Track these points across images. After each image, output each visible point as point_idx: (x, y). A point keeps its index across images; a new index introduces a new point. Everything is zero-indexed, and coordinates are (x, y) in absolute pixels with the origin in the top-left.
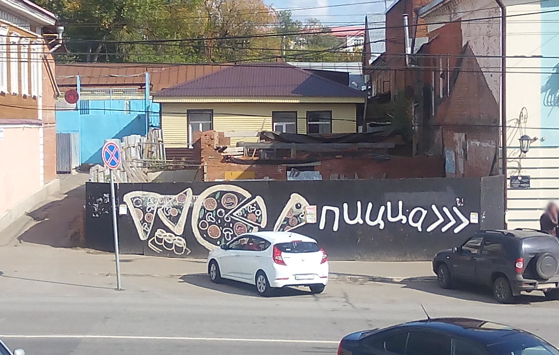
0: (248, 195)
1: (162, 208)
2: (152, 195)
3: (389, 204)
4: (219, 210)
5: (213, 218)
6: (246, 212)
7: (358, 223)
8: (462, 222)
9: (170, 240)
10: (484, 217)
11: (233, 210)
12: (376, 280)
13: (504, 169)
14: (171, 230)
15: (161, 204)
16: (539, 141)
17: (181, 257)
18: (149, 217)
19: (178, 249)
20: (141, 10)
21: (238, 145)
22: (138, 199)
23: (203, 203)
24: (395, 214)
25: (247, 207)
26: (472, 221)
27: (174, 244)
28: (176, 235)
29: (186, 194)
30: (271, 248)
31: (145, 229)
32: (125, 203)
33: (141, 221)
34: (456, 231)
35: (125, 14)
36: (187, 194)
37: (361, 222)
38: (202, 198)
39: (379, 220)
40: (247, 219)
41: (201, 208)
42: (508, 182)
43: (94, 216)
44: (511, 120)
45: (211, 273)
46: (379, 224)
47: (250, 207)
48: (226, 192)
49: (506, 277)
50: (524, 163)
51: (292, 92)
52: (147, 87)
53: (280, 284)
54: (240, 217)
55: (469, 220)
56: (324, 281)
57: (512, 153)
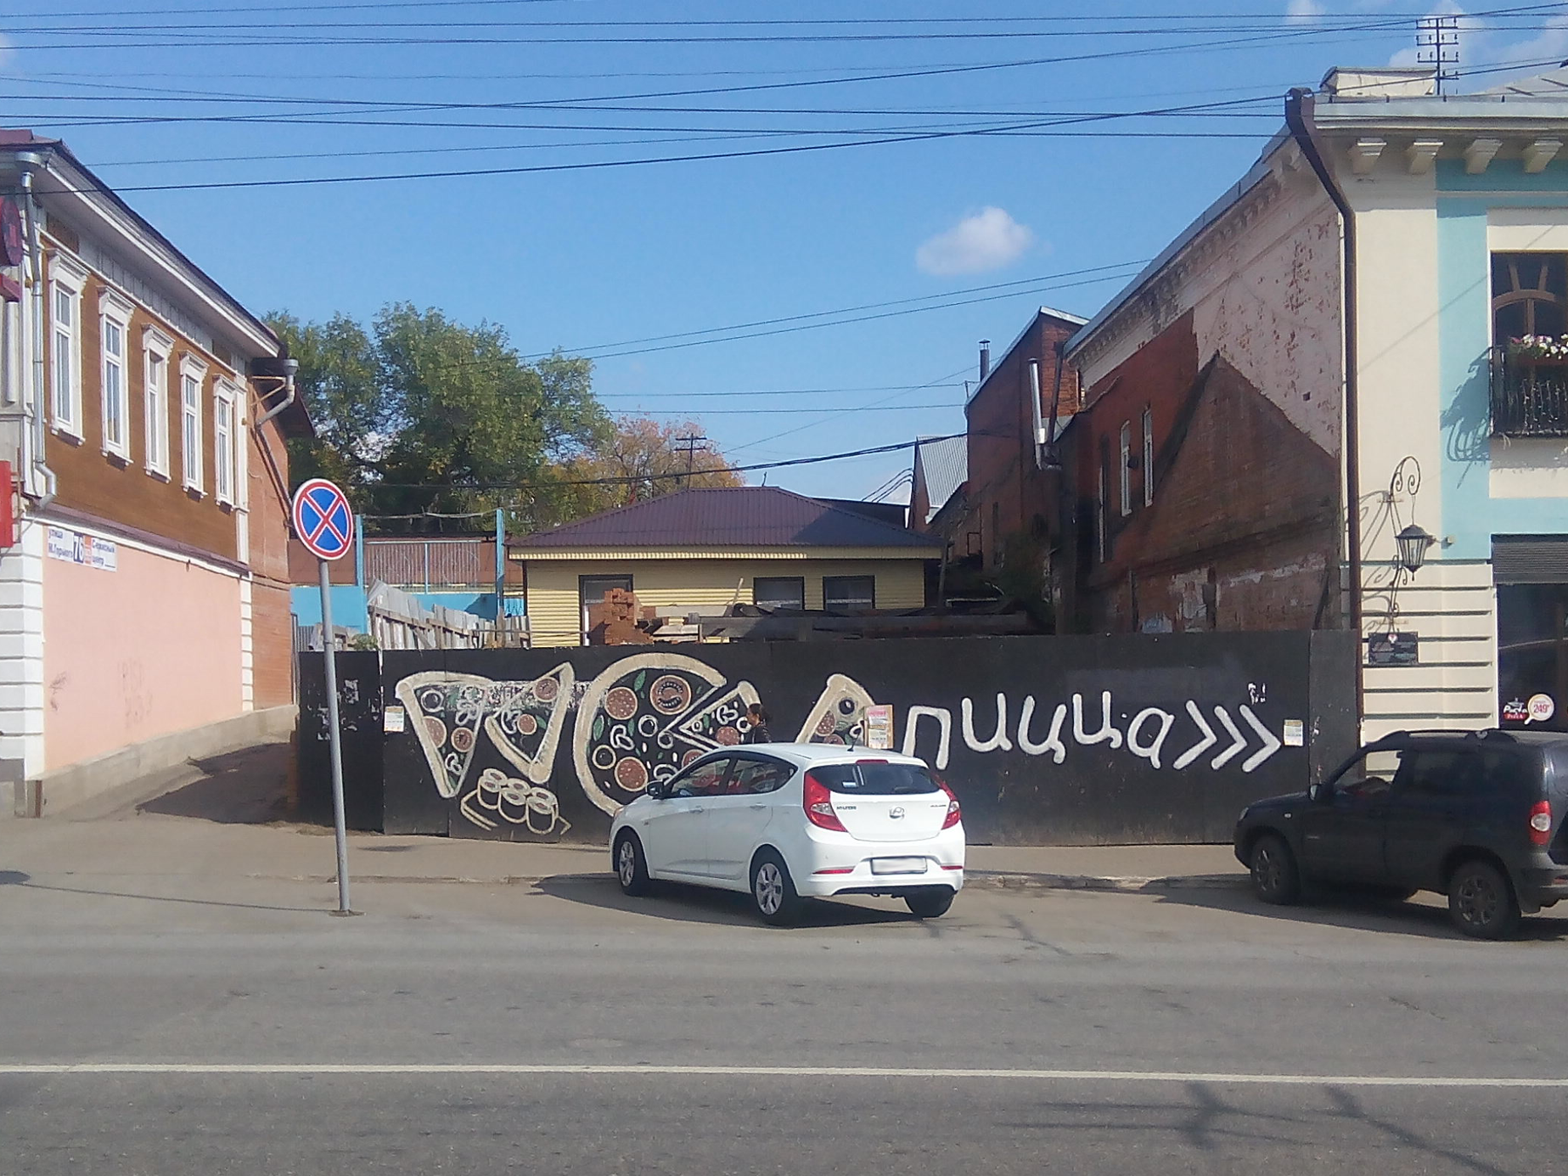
0: (716, 679)
1: (496, 715)
2: (471, 680)
3: (1077, 699)
4: (643, 720)
5: (628, 739)
6: (715, 724)
7: (999, 747)
8: (1263, 745)
9: (516, 798)
10: (1316, 731)
11: (679, 718)
12: (1073, 884)
13: (1355, 615)
14: (519, 771)
15: (494, 705)
16: (1440, 545)
17: (549, 839)
18: (461, 737)
19: (540, 820)
20: (502, 440)
21: (687, 621)
22: (432, 691)
23: (601, 701)
24: (1092, 726)
25: (715, 711)
26: (1288, 742)
27: (527, 807)
28: (532, 785)
29: (559, 680)
30: (798, 780)
31: (452, 769)
32: (398, 702)
33: (440, 749)
34: (1248, 766)
35: (473, 448)
36: (561, 678)
37: (1007, 746)
38: (598, 690)
39: (1053, 741)
40: (715, 740)
41: (598, 715)
42: (1365, 646)
43: (320, 738)
44: (1370, 495)
45: (621, 867)
46: (1052, 752)
47: (722, 710)
48: (661, 672)
49: (1498, 865)
50: (1405, 601)
51: (793, 540)
52: (500, 537)
53: (828, 886)
54: (699, 737)
55: (1281, 739)
56: (951, 879)
57: (1374, 577)
